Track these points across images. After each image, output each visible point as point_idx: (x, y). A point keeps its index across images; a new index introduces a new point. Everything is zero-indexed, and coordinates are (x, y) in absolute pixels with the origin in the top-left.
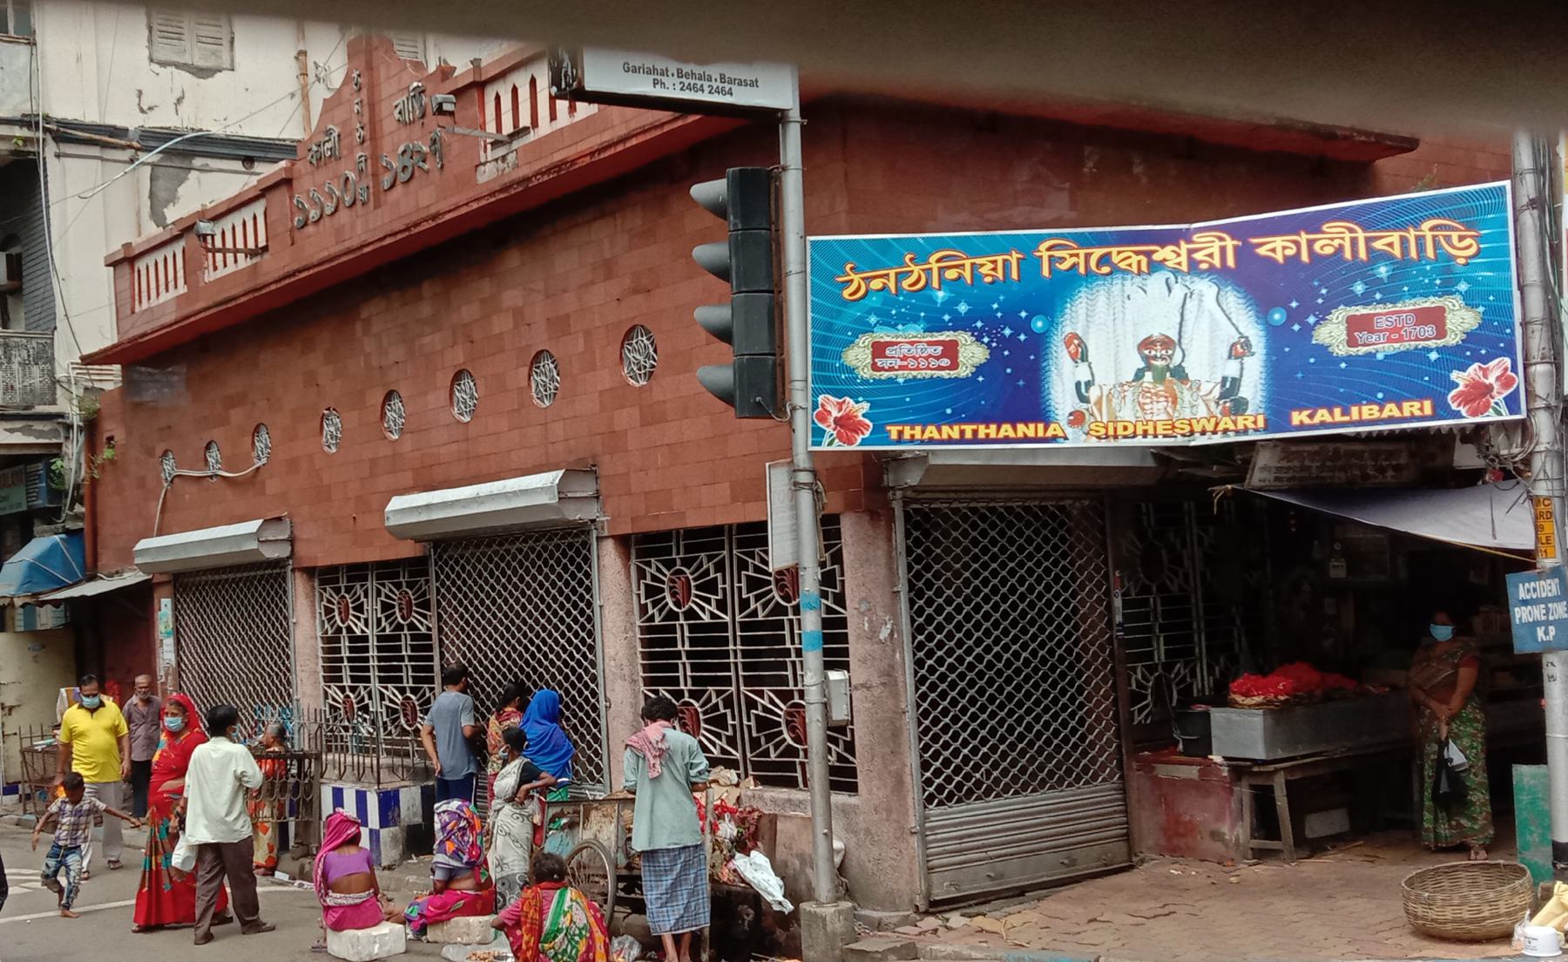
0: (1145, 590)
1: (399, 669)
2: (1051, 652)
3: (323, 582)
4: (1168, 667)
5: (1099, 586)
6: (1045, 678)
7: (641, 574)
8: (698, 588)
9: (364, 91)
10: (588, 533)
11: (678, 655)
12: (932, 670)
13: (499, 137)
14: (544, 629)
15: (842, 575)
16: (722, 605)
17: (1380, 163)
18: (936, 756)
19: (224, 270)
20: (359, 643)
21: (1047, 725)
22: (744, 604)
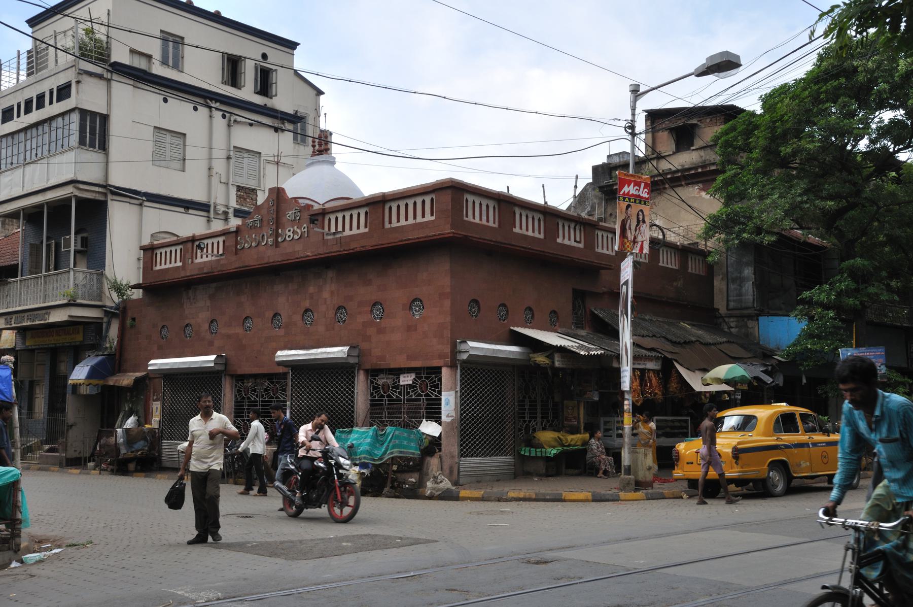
0: (524, 397)
2: (497, 415)
3: (237, 380)
4: (530, 422)
5: (512, 396)
6: (495, 423)
7: (372, 382)
8: (392, 387)
9: (275, 206)
10: (355, 368)
11: (388, 409)
13: (329, 232)
14: (476, 402)
15: (441, 385)
16: (400, 393)
17: (601, 271)
18: (464, 443)
19: (202, 259)
21: (495, 437)
22: (408, 393)
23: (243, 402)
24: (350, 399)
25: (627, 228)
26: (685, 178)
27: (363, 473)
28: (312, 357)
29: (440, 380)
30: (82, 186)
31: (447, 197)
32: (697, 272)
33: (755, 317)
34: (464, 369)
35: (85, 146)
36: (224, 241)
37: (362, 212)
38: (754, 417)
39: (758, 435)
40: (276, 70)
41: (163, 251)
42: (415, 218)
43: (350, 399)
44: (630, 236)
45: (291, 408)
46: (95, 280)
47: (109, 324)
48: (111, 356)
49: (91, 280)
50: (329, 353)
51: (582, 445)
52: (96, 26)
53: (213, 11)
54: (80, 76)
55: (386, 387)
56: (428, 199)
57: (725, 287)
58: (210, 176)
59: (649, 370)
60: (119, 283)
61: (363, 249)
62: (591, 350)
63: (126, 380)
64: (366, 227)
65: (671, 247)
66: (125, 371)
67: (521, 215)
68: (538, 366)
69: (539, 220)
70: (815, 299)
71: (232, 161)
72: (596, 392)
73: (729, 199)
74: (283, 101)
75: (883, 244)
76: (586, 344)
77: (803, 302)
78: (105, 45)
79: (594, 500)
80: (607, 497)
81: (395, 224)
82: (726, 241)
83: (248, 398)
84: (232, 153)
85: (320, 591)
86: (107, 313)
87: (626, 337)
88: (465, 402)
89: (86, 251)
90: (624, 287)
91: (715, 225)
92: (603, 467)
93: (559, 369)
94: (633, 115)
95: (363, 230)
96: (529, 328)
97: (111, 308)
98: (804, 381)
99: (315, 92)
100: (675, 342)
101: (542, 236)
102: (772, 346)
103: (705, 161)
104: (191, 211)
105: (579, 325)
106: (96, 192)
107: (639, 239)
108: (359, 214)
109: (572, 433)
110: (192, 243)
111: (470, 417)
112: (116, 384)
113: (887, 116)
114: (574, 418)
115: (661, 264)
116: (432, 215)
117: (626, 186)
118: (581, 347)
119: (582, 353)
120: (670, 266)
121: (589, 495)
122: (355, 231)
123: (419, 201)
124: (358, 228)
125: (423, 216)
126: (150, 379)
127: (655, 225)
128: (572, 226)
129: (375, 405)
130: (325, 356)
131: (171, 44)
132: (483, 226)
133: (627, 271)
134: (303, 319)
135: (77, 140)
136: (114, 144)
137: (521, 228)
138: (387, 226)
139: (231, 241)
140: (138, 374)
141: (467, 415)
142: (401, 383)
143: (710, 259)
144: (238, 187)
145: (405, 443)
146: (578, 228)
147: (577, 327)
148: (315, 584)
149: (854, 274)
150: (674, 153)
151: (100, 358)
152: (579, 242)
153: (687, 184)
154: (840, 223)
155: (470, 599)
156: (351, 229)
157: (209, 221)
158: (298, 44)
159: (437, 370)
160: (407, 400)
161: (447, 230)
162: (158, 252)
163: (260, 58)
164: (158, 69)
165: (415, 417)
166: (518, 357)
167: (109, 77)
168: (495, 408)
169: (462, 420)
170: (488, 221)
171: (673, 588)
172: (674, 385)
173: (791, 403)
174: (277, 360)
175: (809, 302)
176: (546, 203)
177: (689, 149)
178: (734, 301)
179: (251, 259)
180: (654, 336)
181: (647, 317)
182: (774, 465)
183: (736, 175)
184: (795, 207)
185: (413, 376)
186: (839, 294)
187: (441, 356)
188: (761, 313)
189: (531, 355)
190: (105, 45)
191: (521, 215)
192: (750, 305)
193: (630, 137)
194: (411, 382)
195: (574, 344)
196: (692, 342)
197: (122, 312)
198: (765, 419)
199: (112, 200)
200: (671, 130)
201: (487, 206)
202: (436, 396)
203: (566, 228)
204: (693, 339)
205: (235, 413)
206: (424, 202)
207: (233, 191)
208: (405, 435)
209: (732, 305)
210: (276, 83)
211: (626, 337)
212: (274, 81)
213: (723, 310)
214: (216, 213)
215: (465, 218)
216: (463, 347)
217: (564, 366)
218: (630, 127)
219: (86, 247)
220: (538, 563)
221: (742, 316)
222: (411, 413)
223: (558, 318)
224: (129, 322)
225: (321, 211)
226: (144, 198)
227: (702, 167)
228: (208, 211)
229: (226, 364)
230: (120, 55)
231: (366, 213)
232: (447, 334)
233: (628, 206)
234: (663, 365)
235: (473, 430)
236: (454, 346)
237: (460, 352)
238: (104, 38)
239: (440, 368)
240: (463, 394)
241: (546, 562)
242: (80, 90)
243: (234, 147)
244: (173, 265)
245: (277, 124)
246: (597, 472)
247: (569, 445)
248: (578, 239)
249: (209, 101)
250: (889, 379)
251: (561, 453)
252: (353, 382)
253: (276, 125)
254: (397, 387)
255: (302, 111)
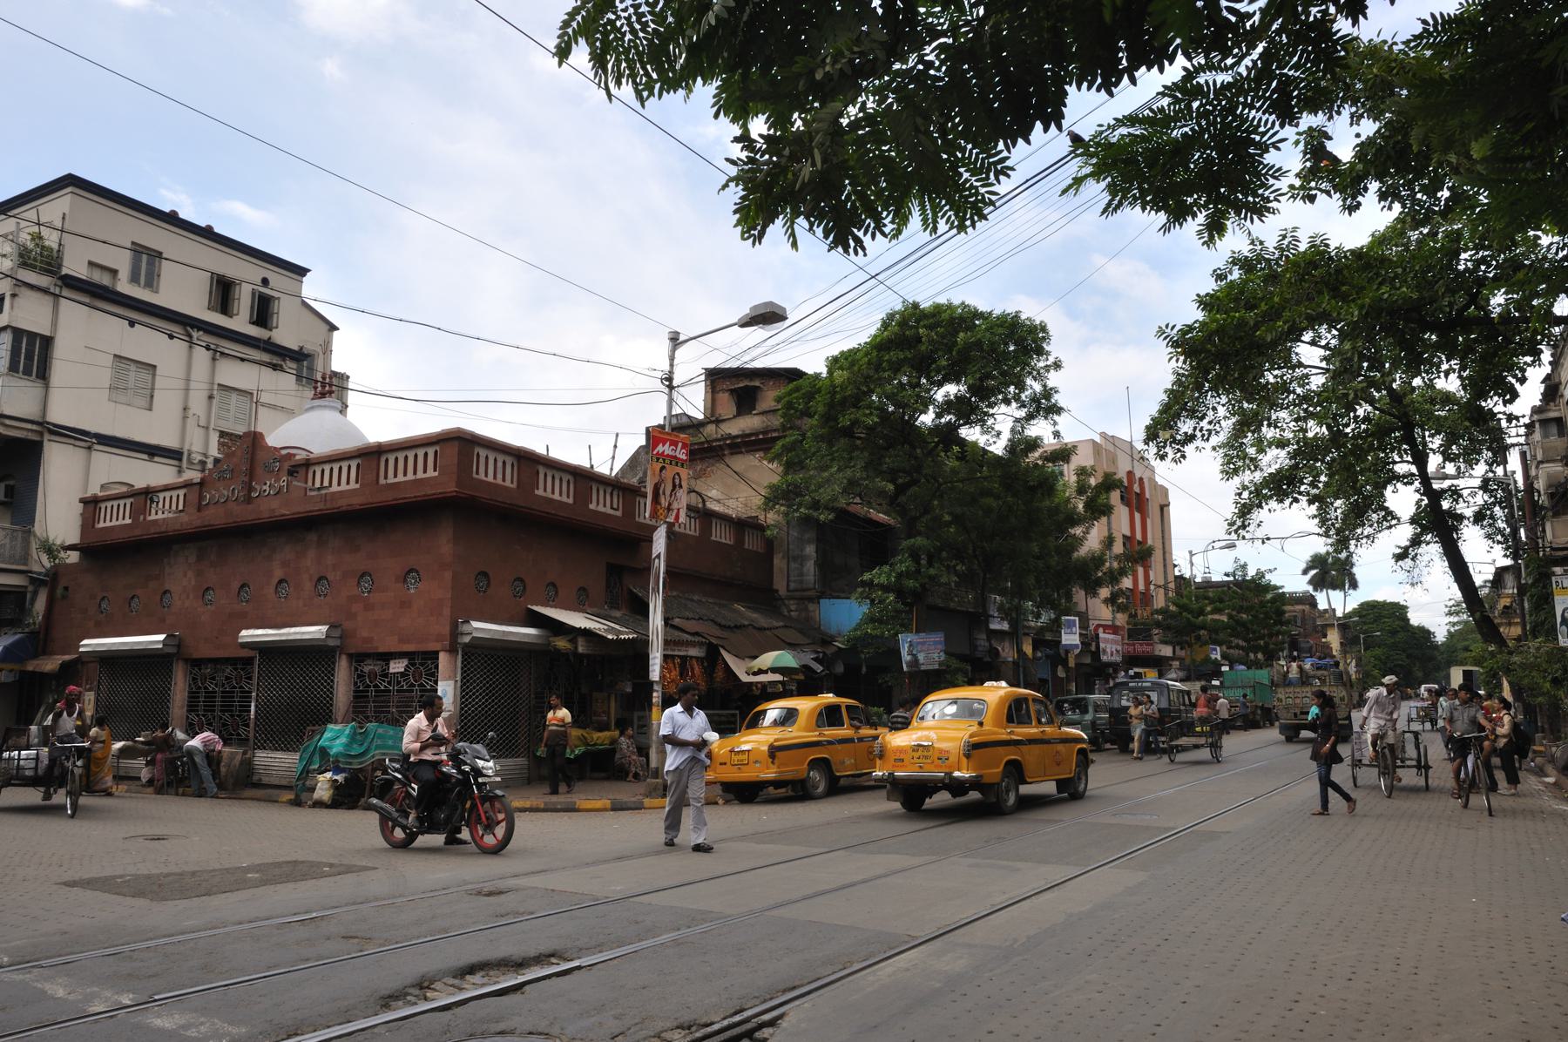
1: (214, 706)
7: (356, 669)
10: (335, 652)
11: (374, 702)
12: (466, 712)
14: (474, 694)
19: (158, 514)
20: (211, 695)
22: (399, 683)
23: (198, 693)
24: (328, 690)
25: (661, 492)
26: (746, 444)
27: (336, 781)
28: (283, 638)
29: (437, 667)
30: (8, 422)
31: (453, 450)
32: (755, 549)
33: (816, 600)
34: (466, 654)
35: (18, 372)
36: (185, 495)
37: (354, 464)
38: (796, 710)
39: (799, 730)
40: (279, 299)
41: (109, 504)
42: (415, 473)
43: (328, 690)
44: (664, 502)
45: (257, 701)
46: (19, 539)
47: (35, 593)
48: (33, 635)
49: (13, 539)
50: (303, 633)
51: (611, 744)
52: (45, 232)
53: (167, 210)
54: (17, 289)
55: (373, 675)
56: (431, 451)
57: (786, 566)
58: (185, 418)
59: (691, 657)
60: (51, 542)
61: (350, 508)
62: (622, 633)
63: (50, 664)
64: (357, 482)
65: (724, 520)
66: (52, 653)
67: (546, 475)
68: (557, 651)
69: (568, 482)
70: (876, 581)
71: (215, 401)
72: (629, 683)
73: (789, 467)
74: (286, 334)
75: (948, 524)
76: (617, 627)
77: (863, 584)
78: (55, 255)
79: (614, 809)
80: (629, 805)
81: (391, 480)
82: (786, 514)
83: (206, 688)
84: (215, 392)
85: (166, 947)
86: (33, 581)
87: (656, 619)
88: (467, 694)
89: (11, 503)
90: (657, 561)
91: (775, 497)
92: (633, 769)
93: (581, 655)
94: (672, 365)
95: (353, 485)
96: (551, 607)
97: (40, 574)
98: (864, 670)
99: (328, 327)
100: (724, 626)
101: (571, 501)
102: (833, 631)
103: (767, 426)
104: (156, 459)
105: (614, 605)
106: (28, 430)
107: (675, 506)
108: (349, 467)
109: (601, 730)
110: (146, 495)
111: (473, 712)
112: (37, 670)
113: (951, 389)
114: (604, 712)
115: (713, 538)
116: (435, 470)
117: (661, 445)
118: (611, 630)
119: (610, 637)
120: (723, 541)
121: (608, 803)
122: (344, 487)
123: (421, 453)
124: (348, 483)
125: (425, 471)
126: (83, 663)
127: (694, 491)
128: (609, 490)
129: (359, 696)
130: (298, 637)
131: (145, 257)
132: (497, 485)
133: (659, 544)
134: (276, 592)
135: (7, 365)
136: (60, 370)
137: (545, 490)
138: (382, 481)
139: (193, 497)
140: (67, 658)
141: (469, 709)
142: (391, 671)
143: (769, 532)
144: (222, 432)
145: (390, 743)
146: (615, 493)
147: (611, 608)
148: (164, 936)
149: (915, 555)
150: (735, 417)
151: (18, 636)
152: (617, 510)
153: (747, 452)
154: (902, 499)
155: (367, 950)
156: (339, 484)
157: (180, 472)
158: (309, 270)
159: (434, 656)
160: (398, 691)
161: (451, 488)
162: (103, 506)
163: (259, 282)
164: (124, 287)
165: (404, 712)
166: (539, 641)
167: (57, 292)
168: (480, 700)
169: (462, 715)
170: (504, 480)
171: (637, 923)
172: (719, 674)
173: (838, 694)
174: (240, 641)
175: (870, 584)
176: (592, 467)
177: (750, 413)
178: (795, 581)
179: (215, 517)
180: (700, 619)
181: (696, 598)
182: (815, 764)
183: (796, 442)
184: (852, 483)
185: (405, 662)
186: (900, 575)
187: (439, 638)
188: (822, 595)
189: (551, 639)
190: (55, 255)
191: (546, 475)
192: (811, 586)
193: (667, 390)
194: (403, 670)
195: (602, 626)
196: (744, 626)
197: (52, 580)
198: (807, 712)
199: (49, 440)
200: (732, 391)
201: (504, 463)
202: (432, 686)
203: (601, 493)
204: (746, 623)
205: (188, 706)
206: (426, 454)
207: (214, 438)
208: (391, 732)
209: (792, 586)
210: (277, 313)
211: (656, 619)
212: (237, 297)
213: (783, 592)
214: (190, 461)
215: (475, 476)
216: (465, 628)
217: (590, 652)
218: (666, 379)
219: (12, 497)
220: (490, 894)
221: (802, 599)
222: (400, 707)
223: (588, 596)
224: (59, 592)
225: (304, 462)
226: (94, 440)
227: (763, 433)
228: (180, 460)
229: (179, 646)
230: (75, 265)
231: (358, 465)
232: (447, 612)
233: (663, 468)
234: (708, 652)
235: (476, 727)
236: (455, 626)
237: (462, 634)
238: (55, 246)
239: (437, 653)
240: (464, 684)
241: (501, 893)
242: (15, 305)
243: (219, 385)
244: (121, 522)
245: (276, 360)
246: (627, 775)
247: (595, 744)
248: (615, 506)
249: (189, 328)
250: (948, 666)
251: (584, 753)
252: (333, 669)
253: (275, 362)
254: (386, 675)
255: (309, 347)
